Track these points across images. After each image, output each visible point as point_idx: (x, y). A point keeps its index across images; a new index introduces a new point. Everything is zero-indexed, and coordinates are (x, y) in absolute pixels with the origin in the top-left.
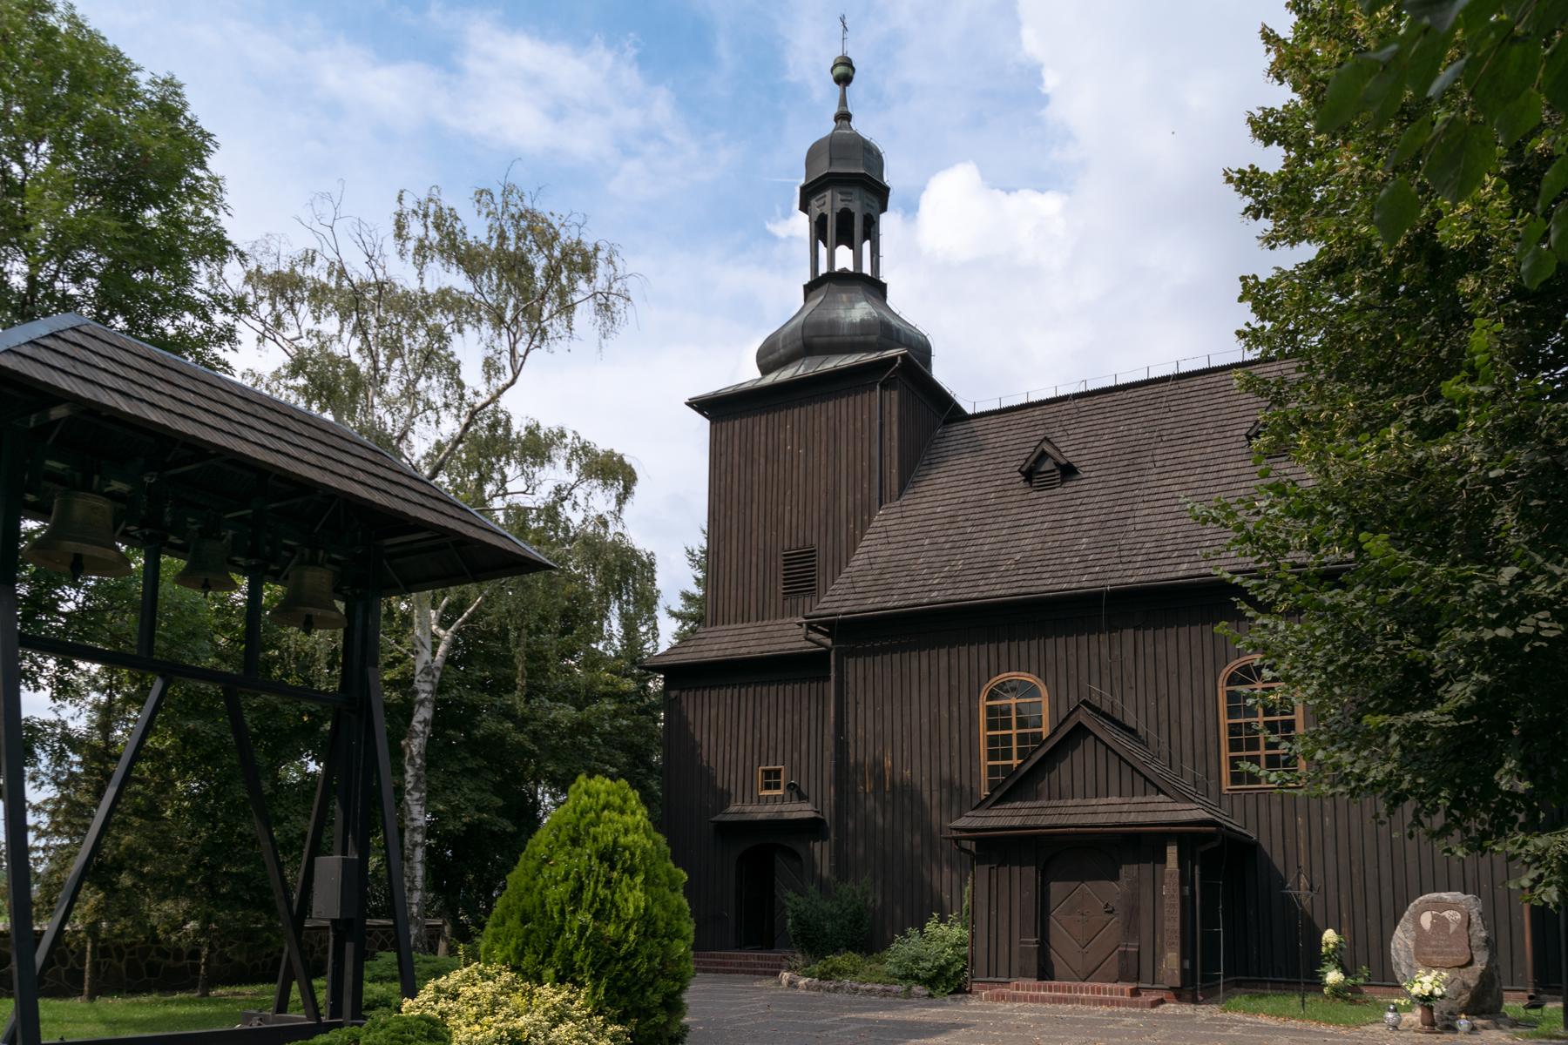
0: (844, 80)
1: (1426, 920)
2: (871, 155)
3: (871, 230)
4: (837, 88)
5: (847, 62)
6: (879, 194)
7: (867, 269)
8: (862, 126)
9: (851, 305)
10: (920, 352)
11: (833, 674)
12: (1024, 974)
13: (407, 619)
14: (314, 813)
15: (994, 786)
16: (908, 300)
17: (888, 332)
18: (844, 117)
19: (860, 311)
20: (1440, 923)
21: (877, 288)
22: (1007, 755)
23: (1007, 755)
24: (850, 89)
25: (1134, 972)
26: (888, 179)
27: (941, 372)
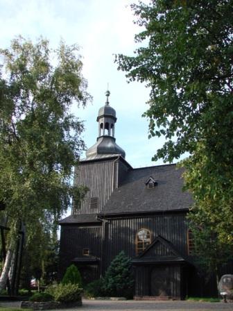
0: (108, 95)
1: (224, 280)
2: (113, 111)
3: (112, 126)
4: (106, 97)
5: (108, 92)
6: (115, 120)
7: (111, 135)
8: (111, 105)
9: (108, 142)
10: (123, 154)
11: (7, 260)
12: (146, 295)
13: (148, 237)
14: (97, 227)
15: (139, 254)
16: (120, 143)
17: (116, 150)
18: (108, 103)
19: (110, 145)
20: (227, 280)
21: (113, 139)
22: (142, 247)
23: (142, 247)
24: (109, 97)
25: (169, 295)
26: (117, 116)
27: (127, 159)
